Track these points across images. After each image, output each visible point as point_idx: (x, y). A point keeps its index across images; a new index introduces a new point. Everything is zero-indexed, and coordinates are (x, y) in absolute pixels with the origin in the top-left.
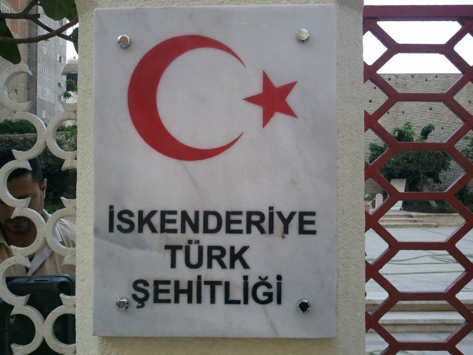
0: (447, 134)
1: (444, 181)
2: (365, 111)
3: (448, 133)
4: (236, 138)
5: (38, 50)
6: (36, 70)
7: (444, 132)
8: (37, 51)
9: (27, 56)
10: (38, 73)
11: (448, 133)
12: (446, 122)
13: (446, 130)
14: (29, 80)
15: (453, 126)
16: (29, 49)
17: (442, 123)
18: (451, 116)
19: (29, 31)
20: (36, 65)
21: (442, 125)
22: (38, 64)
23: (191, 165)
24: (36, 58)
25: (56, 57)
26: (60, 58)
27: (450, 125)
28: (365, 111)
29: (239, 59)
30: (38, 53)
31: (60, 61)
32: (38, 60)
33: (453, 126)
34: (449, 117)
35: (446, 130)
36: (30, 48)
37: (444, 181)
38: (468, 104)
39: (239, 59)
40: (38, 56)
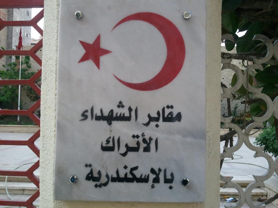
0: (226, 82)
1: (224, 110)
2: (221, 82)
3: (226, 81)
4: (120, 25)
5: (13, 30)
6: (12, 41)
7: (224, 81)
8: (12, 30)
9: (6, 33)
10: (13, 43)
11: (226, 81)
12: (226, 75)
13: (225, 80)
14: (7, 47)
15: (229, 77)
16: (8, 29)
17: (224, 76)
18: (228, 71)
19: (8, 18)
20: (12, 38)
21: (223, 76)
22: (13, 38)
23: (134, 12)
24: (12, 34)
25: (25, 33)
26: (27, 35)
27: (228, 77)
28: (221, 82)
29: (116, 78)
30: (13, 31)
31: (27, 36)
32: (13, 36)
33: (229, 77)
34: (228, 72)
35: (225, 80)
36: (8, 28)
37: (224, 110)
38: (239, 64)
39: (116, 78)
40: (13, 33)
